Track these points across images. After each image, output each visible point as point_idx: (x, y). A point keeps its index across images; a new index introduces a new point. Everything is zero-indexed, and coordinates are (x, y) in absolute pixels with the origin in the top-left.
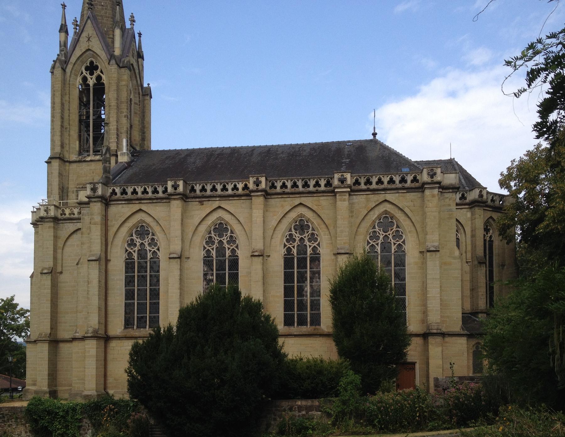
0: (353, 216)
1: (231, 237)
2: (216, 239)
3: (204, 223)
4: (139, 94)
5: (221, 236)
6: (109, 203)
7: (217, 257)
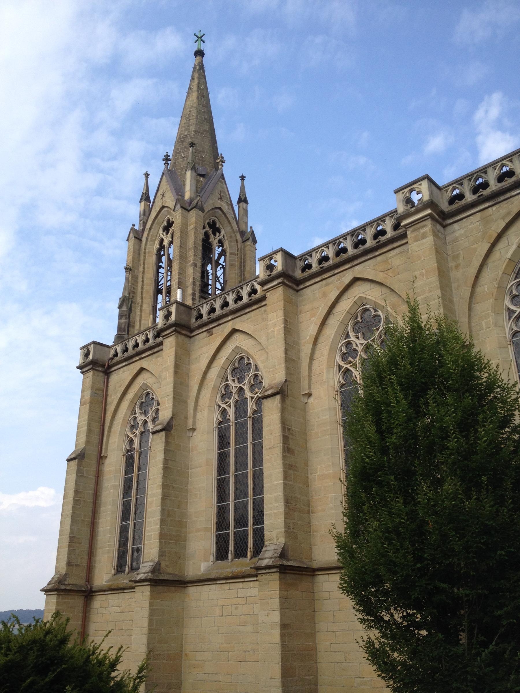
0: (460, 264)
1: (256, 376)
2: (234, 386)
3: (215, 364)
4: (237, 242)
5: (241, 380)
6: (108, 372)
7: (236, 419)
